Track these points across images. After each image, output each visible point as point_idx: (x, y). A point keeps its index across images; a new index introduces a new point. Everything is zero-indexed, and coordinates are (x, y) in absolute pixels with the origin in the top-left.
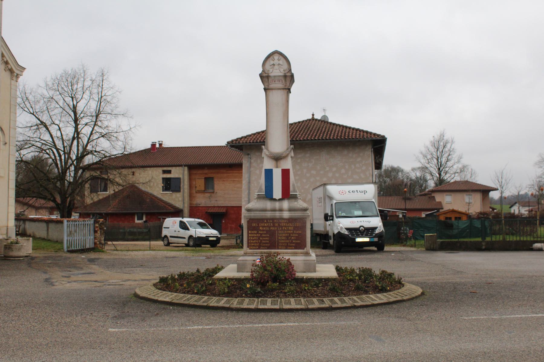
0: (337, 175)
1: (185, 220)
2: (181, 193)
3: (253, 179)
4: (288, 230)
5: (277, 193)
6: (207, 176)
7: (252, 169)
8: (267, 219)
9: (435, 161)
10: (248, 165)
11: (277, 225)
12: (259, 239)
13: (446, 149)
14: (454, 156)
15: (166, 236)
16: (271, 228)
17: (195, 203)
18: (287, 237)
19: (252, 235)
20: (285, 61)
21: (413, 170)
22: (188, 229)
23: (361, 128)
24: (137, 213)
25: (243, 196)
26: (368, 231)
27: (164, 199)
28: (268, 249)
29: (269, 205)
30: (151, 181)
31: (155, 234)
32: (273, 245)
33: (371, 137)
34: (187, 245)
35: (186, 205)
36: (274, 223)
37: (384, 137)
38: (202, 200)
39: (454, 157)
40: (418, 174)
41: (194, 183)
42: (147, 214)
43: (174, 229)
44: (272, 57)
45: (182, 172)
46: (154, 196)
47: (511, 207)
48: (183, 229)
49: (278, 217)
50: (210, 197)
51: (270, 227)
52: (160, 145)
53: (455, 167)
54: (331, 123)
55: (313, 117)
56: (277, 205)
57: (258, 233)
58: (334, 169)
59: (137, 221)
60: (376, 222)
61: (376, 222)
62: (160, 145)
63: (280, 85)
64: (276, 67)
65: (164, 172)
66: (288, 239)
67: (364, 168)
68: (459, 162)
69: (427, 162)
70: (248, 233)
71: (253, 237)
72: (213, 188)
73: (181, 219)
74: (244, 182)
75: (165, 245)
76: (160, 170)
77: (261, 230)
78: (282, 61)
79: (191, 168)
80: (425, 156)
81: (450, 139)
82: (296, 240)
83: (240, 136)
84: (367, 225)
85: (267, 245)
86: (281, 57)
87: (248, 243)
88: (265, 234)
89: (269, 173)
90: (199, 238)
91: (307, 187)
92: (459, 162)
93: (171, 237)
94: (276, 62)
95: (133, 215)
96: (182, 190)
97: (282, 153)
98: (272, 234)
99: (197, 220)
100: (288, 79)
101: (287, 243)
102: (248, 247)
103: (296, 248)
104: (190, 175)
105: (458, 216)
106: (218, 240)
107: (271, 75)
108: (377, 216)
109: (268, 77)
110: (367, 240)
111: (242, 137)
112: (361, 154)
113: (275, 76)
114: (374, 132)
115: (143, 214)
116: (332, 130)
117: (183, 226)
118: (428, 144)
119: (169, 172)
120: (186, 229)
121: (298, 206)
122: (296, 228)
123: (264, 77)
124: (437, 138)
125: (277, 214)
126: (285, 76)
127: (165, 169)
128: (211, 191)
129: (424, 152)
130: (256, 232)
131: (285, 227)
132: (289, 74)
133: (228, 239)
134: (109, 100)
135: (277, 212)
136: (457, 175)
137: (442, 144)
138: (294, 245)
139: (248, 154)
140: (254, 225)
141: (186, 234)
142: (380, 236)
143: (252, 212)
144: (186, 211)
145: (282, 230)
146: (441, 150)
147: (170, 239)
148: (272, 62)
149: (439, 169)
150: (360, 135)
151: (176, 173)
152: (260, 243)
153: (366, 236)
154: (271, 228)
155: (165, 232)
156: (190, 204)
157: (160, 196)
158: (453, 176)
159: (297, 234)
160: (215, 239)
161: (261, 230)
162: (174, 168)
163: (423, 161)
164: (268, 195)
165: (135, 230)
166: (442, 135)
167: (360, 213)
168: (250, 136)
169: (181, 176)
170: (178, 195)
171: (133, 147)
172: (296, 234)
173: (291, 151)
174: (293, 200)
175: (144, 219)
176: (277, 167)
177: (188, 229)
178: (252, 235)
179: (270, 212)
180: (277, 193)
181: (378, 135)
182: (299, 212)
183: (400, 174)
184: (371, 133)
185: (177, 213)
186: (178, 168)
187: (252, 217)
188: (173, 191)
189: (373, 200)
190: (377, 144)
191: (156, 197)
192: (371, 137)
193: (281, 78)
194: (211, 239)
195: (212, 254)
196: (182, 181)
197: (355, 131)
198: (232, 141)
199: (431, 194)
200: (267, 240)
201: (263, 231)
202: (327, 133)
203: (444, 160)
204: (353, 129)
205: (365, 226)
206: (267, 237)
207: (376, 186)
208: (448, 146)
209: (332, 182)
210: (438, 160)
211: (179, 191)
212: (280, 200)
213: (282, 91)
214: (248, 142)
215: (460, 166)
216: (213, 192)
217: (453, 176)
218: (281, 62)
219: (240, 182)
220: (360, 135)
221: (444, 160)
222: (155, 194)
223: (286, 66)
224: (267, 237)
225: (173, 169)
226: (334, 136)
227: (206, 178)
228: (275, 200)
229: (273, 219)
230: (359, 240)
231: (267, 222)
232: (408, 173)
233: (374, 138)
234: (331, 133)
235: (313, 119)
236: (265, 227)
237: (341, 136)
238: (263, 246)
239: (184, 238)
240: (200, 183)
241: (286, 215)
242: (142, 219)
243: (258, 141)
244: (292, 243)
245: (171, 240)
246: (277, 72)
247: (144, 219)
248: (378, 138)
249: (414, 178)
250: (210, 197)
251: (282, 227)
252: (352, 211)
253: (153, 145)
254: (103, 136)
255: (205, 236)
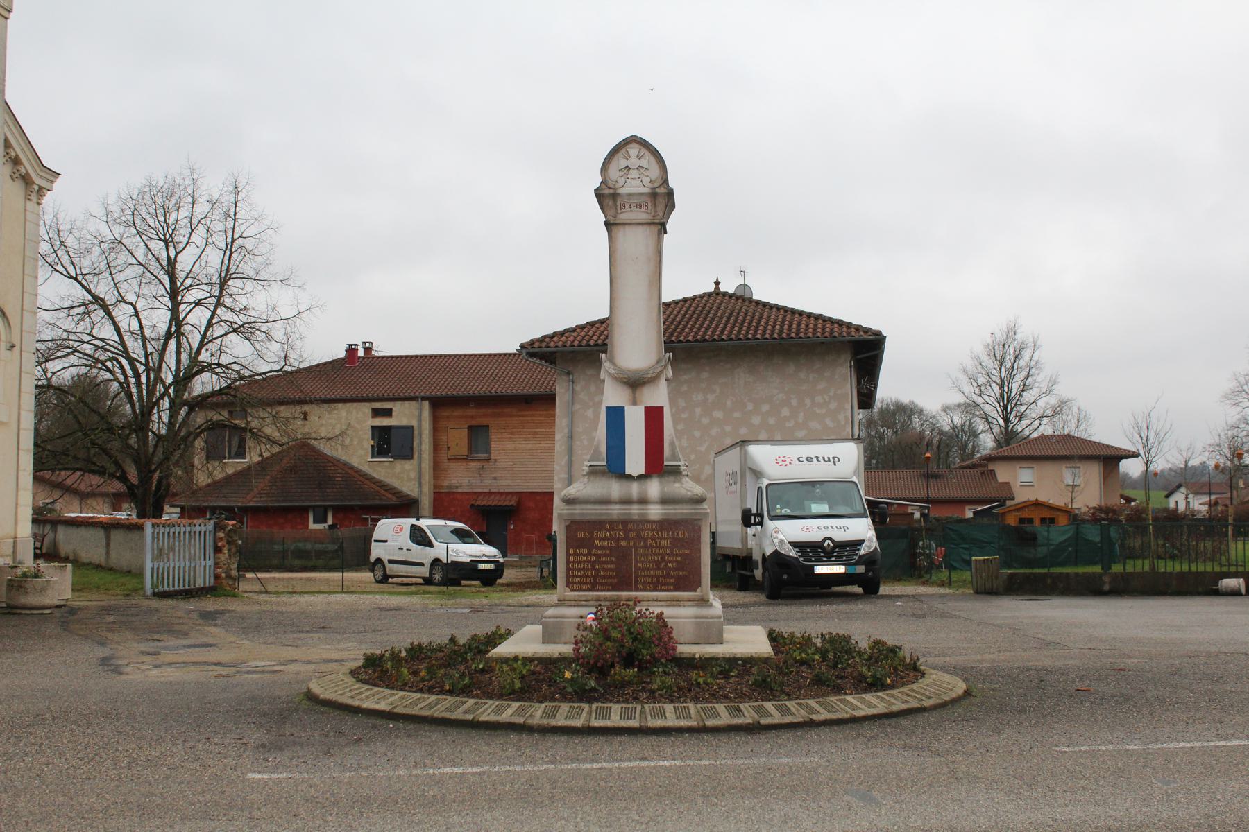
0: (772, 421)
1: (424, 523)
2: (415, 462)
3: (580, 428)
4: (660, 547)
5: (635, 462)
6: (474, 423)
7: (577, 407)
8: (611, 522)
9: (996, 389)
10: (568, 397)
11: (634, 534)
12: (593, 568)
13: (1022, 363)
14: (1039, 379)
15: (379, 561)
16: (621, 543)
17: (446, 483)
18: (658, 563)
19: (578, 559)
20: (652, 159)
21: (946, 409)
22: (430, 545)
23: (827, 314)
24: (314, 508)
25: (557, 467)
26: (844, 550)
27: (375, 475)
28: (613, 590)
29: (615, 488)
30: (345, 433)
31: (355, 555)
32: (624, 582)
33: (849, 334)
34: (428, 581)
35: (426, 489)
36: (626, 531)
37: (878, 333)
38: (462, 479)
39: (1040, 381)
40: (958, 420)
41: (445, 438)
42: (337, 510)
43: (398, 544)
44: (623, 151)
45: (416, 413)
46: (352, 468)
47: (1168, 496)
48: (418, 543)
49: (636, 517)
50: (480, 471)
51: (617, 540)
52: (368, 350)
53: (1041, 403)
54: (758, 302)
55: (717, 288)
56: (634, 489)
57: (589, 554)
58: (765, 408)
59: (312, 526)
60: (861, 529)
61: (861, 529)
62: (368, 350)
63: (642, 216)
64: (633, 174)
65: (377, 413)
66: (659, 568)
67: (833, 405)
68: (1049, 391)
69: (977, 391)
70: (568, 555)
71: (580, 562)
72: (488, 451)
73: (413, 521)
74: (558, 437)
75: (378, 582)
76: (366, 408)
77: (596, 548)
78: (648, 161)
79: (438, 403)
80: (972, 379)
81: (1031, 339)
82: (677, 569)
83: (550, 332)
84: (840, 536)
85: (610, 581)
86: (644, 151)
87: (568, 576)
88: (606, 555)
89: (616, 417)
90: (456, 565)
91: (703, 448)
92: (1049, 391)
93: (391, 561)
94: (633, 162)
95: (303, 511)
96: (416, 456)
97: (646, 371)
98: (622, 555)
99: (449, 523)
100: (661, 202)
101: (658, 577)
102: (567, 586)
103: (677, 588)
104: (435, 419)
105: (1047, 515)
106: (499, 569)
107: (621, 191)
108: (863, 516)
109: (615, 196)
110: (840, 569)
111: (555, 334)
112: (827, 374)
113: (630, 195)
114: (856, 322)
115: (326, 509)
116: (761, 317)
117: (419, 537)
118: (980, 350)
119: (388, 413)
120: (425, 545)
121: (683, 492)
122: (676, 542)
123: (606, 197)
124: (1000, 337)
125: (635, 510)
126: (654, 195)
127: (378, 405)
128: (483, 456)
129: (971, 370)
130: (586, 551)
131: (653, 539)
132: (662, 190)
133: (521, 567)
134: (249, 247)
135: (635, 507)
136: (1045, 421)
137: (1011, 350)
138: (673, 580)
139: (568, 373)
140: (581, 535)
141: (425, 555)
142: (869, 560)
143: (577, 507)
144: (426, 503)
145: (646, 547)
146: (1009, 365)
147: (388, 566)
148: (623, 163)
149: (1005, 408)
150: (823, 329)
151: (403, 415)
152: (595, 577)
153: (838, 561)
154: (621, 543)
155: (376, 551)
156: (435, 486)
157: (365, 468)
158: (1037, 423)
159: (680, 555)
160: (491, 566)
161: (596, 548)
162: (398, 404)
163: (968, 389)
164: (615, 466)
165: (309, 546)
166: (1012, 331)
167: (823, 508)
168: (573, 330)
169: (414, 423)
170: (408, 466)
171: (305, 355)
172: (677, 555)
173: (666, 366)
174: (671, 478)
175: (330, 521)
176: (634, 403)
177: (430, 545)
178: (578, 559)
179: (617, 507)
180: (635, 462)
181: (867, 330)
182: (685, 506)
183: (915, 419)
184: (849, 325)
185: (405, 507)
186: (407, 403)
187: (577, 518)
188: (396, 457)
189: (854, 479)
190: (864, 351)
191: (358, 471)
192: (849, 334)
193: (643, 199)
194: (482, 566)
195: (485, 601)
196: (416, 432)
197: (812, 321)
198: (532, 342)
199: (985, 466)
200: (611, 570)
201: (603, 548)
202: (750, 324)
203: (1015, 387)
204: (810, 315)
205: (836, 539)
206: (612, 563)
207: (861, 446)
208: (1026, 355)
209: (761, 438)
210: (1001, 387)
211: (409, 456)
212: (640, 477)
213: (645, 227)
214: (568, 344)
215: (1053, 401)
216: (488, 460)
217: (1037, 423)
218: (644, 163)
219: (551, 436)
220: (823, 329)
221: (1015, 387)
222: (355, 462)
223: (655, 172)
224: (612, 563)
225: (397, 407)
226: (764, 331)
227: (470, 428)
228: (630, 477)
229: (625, 522)
230: (820, 570)
231: (612, 529)
232: (934, 417)
233: (857, 337)
234: (758, 324)
235: (717, 292)
236: (607, 539)
237: (781, 332)
238: (603, 584)
239: (422, 565)
240: (458, 439)
241: (655, 512)
242: (325, 521)
243: (592, 343)
244: (668, 576)
245: (392, 569)
246: (634, 185)
247: (330, 521)
248: (866, 337)
249: (947, 428)
250: (480, 471)
251: (645, 540)
252: (806, 503)
253: (352, 350)
254: (235, 331)
255: (468, 560)
